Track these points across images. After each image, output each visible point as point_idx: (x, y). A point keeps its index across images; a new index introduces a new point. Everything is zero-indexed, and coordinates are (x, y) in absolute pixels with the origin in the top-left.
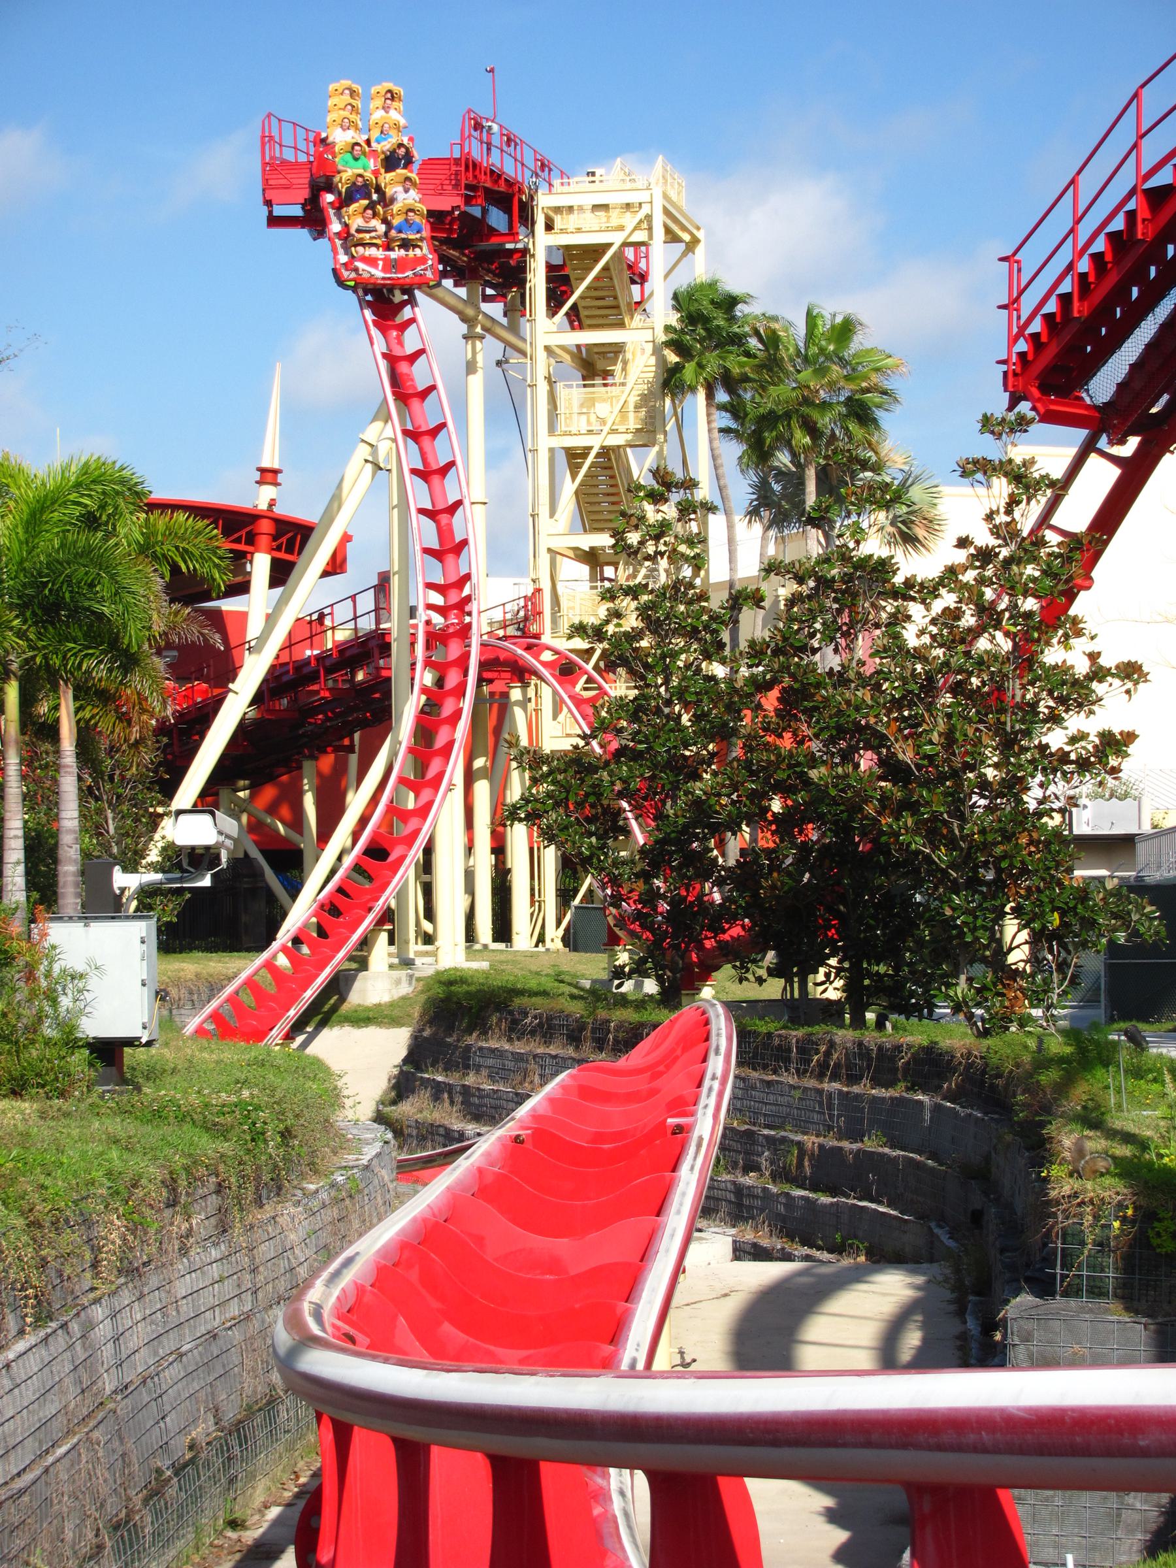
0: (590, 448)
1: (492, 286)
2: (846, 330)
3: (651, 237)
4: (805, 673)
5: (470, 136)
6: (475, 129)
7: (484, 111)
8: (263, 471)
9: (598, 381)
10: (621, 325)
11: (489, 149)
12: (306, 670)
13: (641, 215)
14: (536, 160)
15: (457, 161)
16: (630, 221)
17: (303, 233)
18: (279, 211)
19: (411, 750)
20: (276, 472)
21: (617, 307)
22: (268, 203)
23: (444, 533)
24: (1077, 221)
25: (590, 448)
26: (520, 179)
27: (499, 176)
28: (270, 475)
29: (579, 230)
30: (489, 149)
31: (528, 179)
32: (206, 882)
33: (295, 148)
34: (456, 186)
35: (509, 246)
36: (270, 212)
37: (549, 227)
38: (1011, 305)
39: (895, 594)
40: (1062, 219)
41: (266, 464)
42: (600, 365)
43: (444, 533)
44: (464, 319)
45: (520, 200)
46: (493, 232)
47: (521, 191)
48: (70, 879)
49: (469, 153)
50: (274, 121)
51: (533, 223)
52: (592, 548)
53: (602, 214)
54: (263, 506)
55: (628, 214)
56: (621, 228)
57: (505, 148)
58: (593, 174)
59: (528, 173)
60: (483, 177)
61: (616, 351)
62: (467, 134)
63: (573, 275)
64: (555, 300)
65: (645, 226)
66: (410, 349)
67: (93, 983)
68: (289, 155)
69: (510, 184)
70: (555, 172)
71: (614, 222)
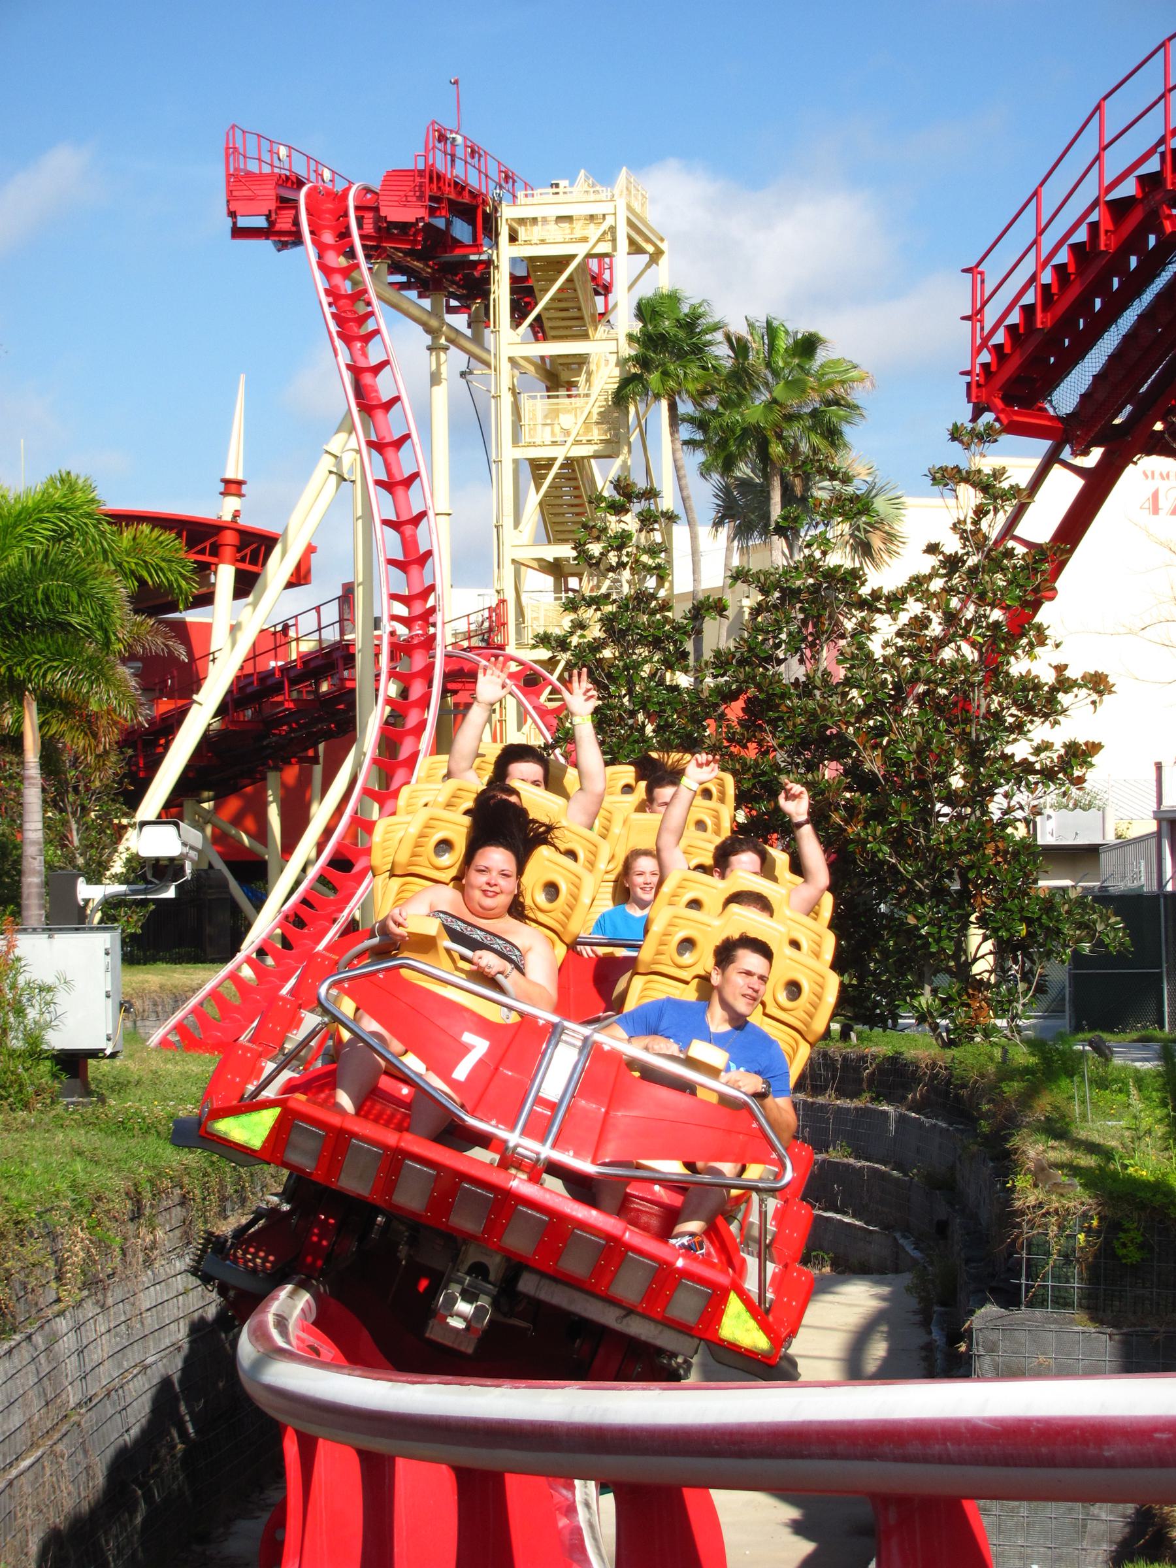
0: (555, 459)
1: (457, 298)
2: (808, 346)
3: (614, 248)
4: (771, 683)
5: (434, 147)
6: (440, 141)
7: (448, 123)
8: (227, 482)
9: (562, 392)
10: (585, 336)
11: (453, 161)
12: (270, 682)
13: (605, 226)
14: (500, 171)
15: (421, 173)
16: (594, 232)
17: (266, 246)
18: (243, 222)
19: (375, 761)
20: (240, 483)
21: (581, 318)
22: (232, 214)
23: (409, 544)
24: (1040, 232)
25: (555, 459)
26: (484, 191)
27: (463, 188)
28: (233, 486)
29: (543, 242)
30: (453, 161)
31: (492, 191)
32: (171, 893)
33: (260, 160)
34: (421, 198)
35: (473, 257)
36: (235, 223)
37: (513, 239)
38: (975, 316)
39: (862, 604)
40: (1025, 230)
41: (230, 475)
42: (564, 376)
43: (409, 544)
44: (429, 330)
45: (484, 212)
46: (457, 243)
47: (485, 203)
48: (34, 890)
49: (433, 165)
50: (238, 133)
51: (497, 235)
52: (556, 559)
53: (566, 225)
54: (227, 517)
55: (592, 226)
56: (585, 240)
57: (469, 160)
58: (557, 186)
59: (492, 185)
60: (447, 189)
61: (580, 361)
62: (431, 145)
63: (537, 286)
64: (521, 305)
65: (609, 237)
66: (374, 361)
67: (61, 997)
68: (253, 167)
69: (474, 195)
70: (519, 184)
71: (578, 234)
